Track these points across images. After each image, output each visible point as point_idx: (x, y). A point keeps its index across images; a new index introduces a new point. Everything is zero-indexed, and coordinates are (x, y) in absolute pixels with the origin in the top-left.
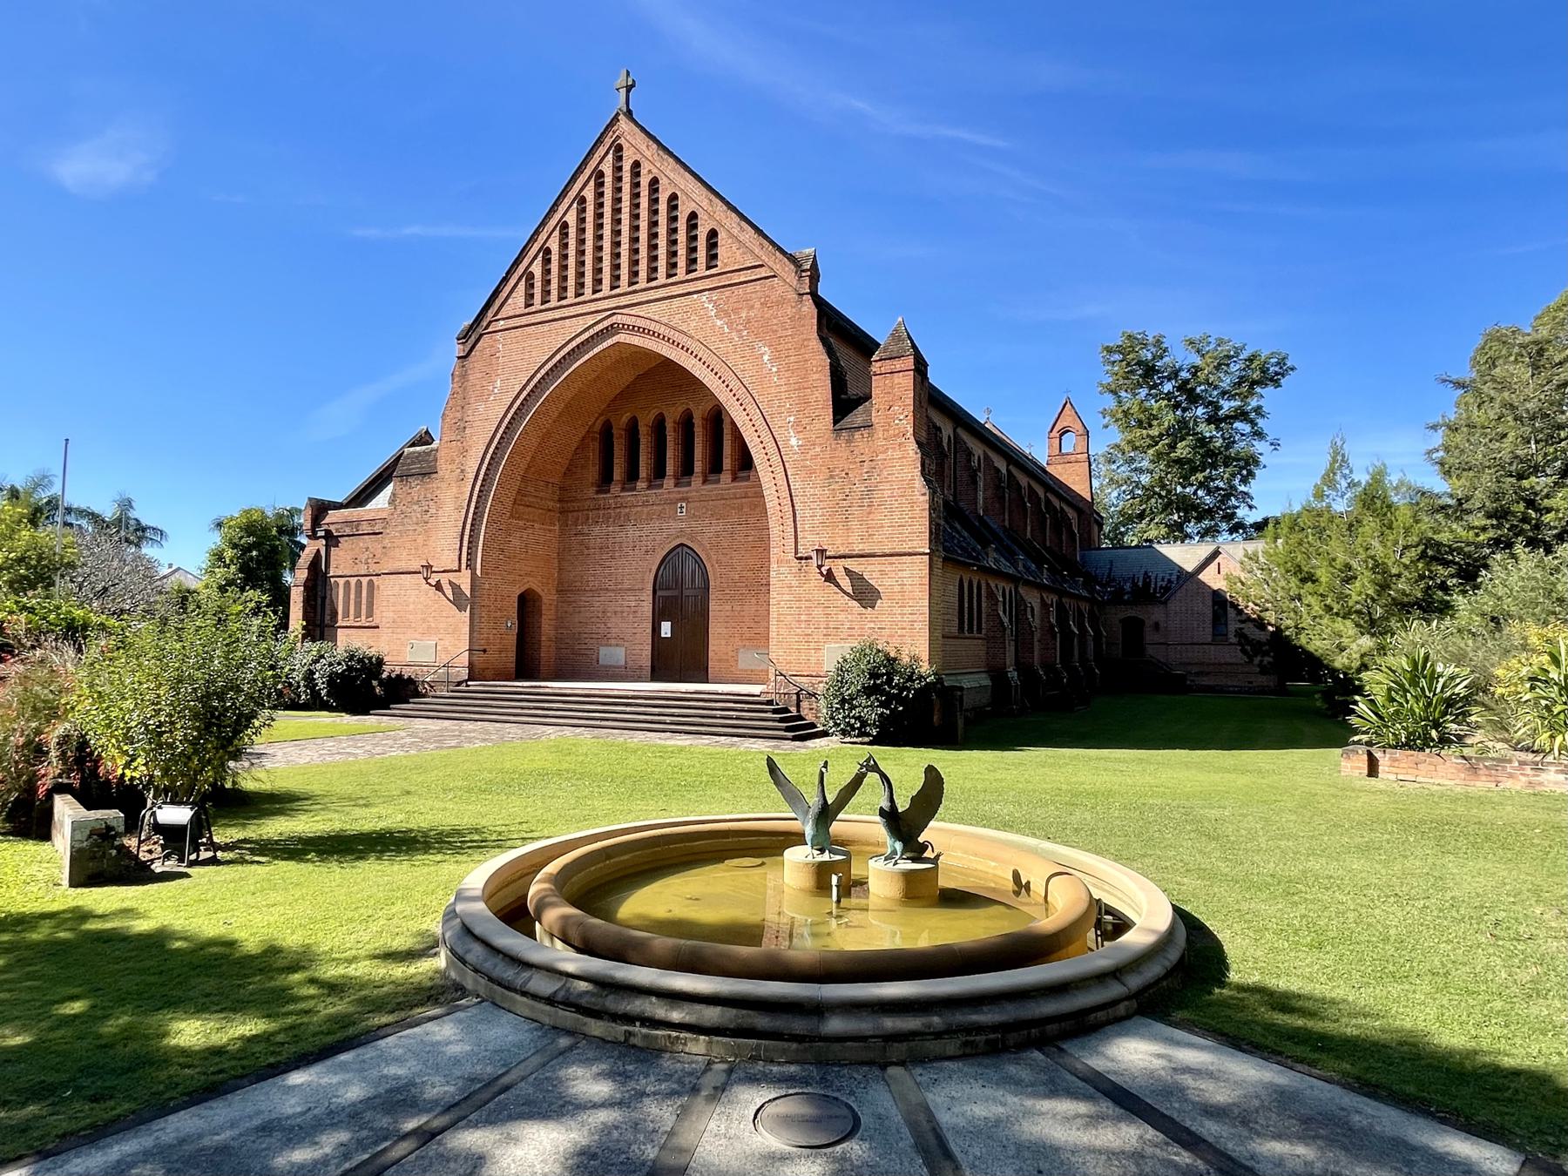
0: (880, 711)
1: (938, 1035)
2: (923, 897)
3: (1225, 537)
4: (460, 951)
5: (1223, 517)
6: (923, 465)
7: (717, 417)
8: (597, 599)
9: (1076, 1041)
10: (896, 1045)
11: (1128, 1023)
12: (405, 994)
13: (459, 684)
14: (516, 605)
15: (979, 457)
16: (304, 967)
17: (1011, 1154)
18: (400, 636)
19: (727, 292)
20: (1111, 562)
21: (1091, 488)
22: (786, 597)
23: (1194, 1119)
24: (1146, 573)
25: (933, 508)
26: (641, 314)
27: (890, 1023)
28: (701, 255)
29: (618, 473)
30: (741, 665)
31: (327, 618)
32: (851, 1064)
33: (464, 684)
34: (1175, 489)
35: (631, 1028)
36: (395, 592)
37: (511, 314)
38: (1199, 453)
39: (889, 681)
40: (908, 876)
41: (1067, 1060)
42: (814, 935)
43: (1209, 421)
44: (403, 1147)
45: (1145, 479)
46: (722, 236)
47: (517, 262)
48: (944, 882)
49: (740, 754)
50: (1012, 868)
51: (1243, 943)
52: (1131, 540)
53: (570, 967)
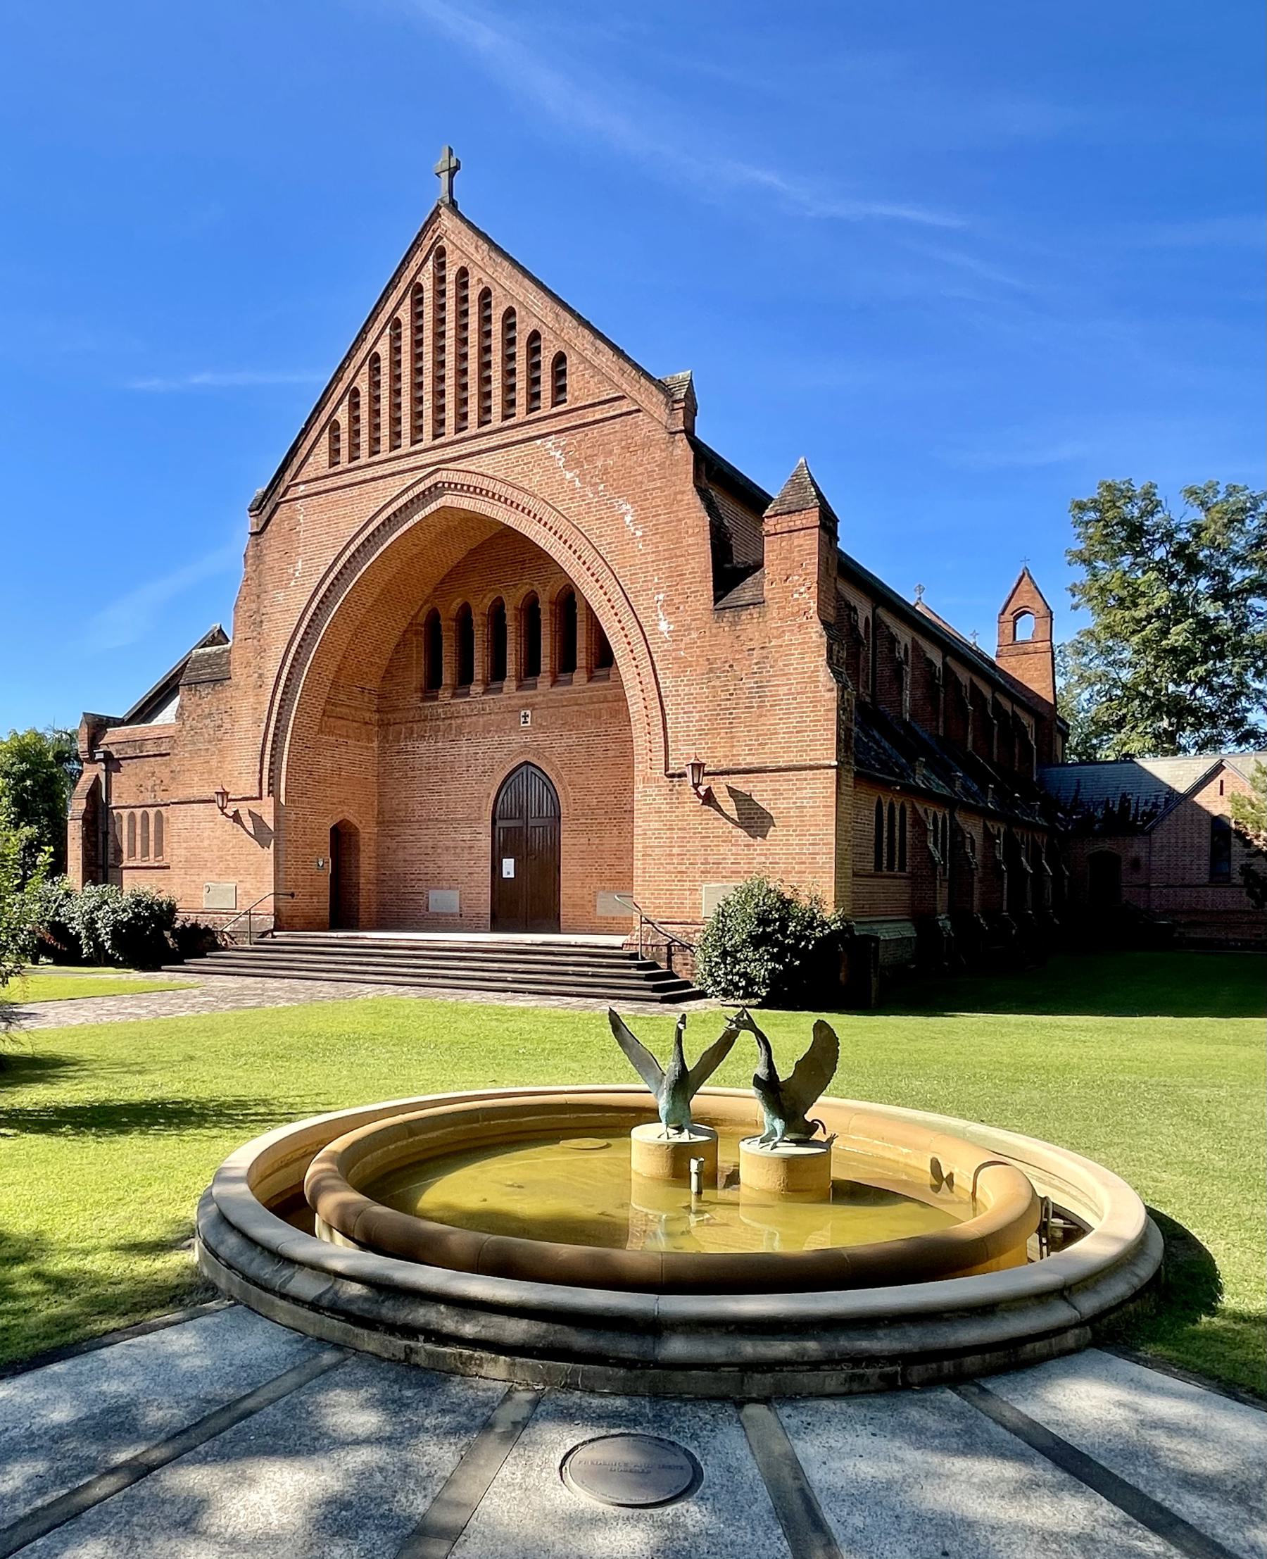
0: (770, 965)
1: (815, 1365)
2: (810, 1190)
3: (1231, 749)
4: (211, 1241)
5: (1229, 723)
6: (830, 651)
7: (569, 600)
8: (425, 832)
9: (1004, 1379)
10: (757, 1376)
11: (1076, 1358)
12: (143, 1294)
13: (264, 934)
14: (328, 840)
15: (906, 645)
16: (32, 1258)
17: (906, 1526)
18: (195, 878)
19: (579, 435)
20: (1078, 781)
21: (1054, 687)
22: (656, 825)
23: (1167, 1491)
24: (1124, 795)
25: (842, 707)
26: (472, 468)
27: (750, 1348)
28: (546, 387)
29: (447, 677)
30: (600, 912)
31: (111, 857)
32: (697, 1399)
33: (270, 935)
34: (1167, 688)
35: (412, 1344)
36: (187, 825)
37: (313, 476)
38: (1200, 639)
39: (784, 928)
40: (790, 1163)
41: (991, 1405)
42: (669, 1235)
43: (1215, 597)
44: (111, 1482)
45: (1126, 675)
46: (572, 360)
47: (318, 409)
48: (838, 1172)
49: (594, 1018)
50: (930, 1157)
51: (1244, 1258)
52: (1106, 753)
53: (339, 1265)
